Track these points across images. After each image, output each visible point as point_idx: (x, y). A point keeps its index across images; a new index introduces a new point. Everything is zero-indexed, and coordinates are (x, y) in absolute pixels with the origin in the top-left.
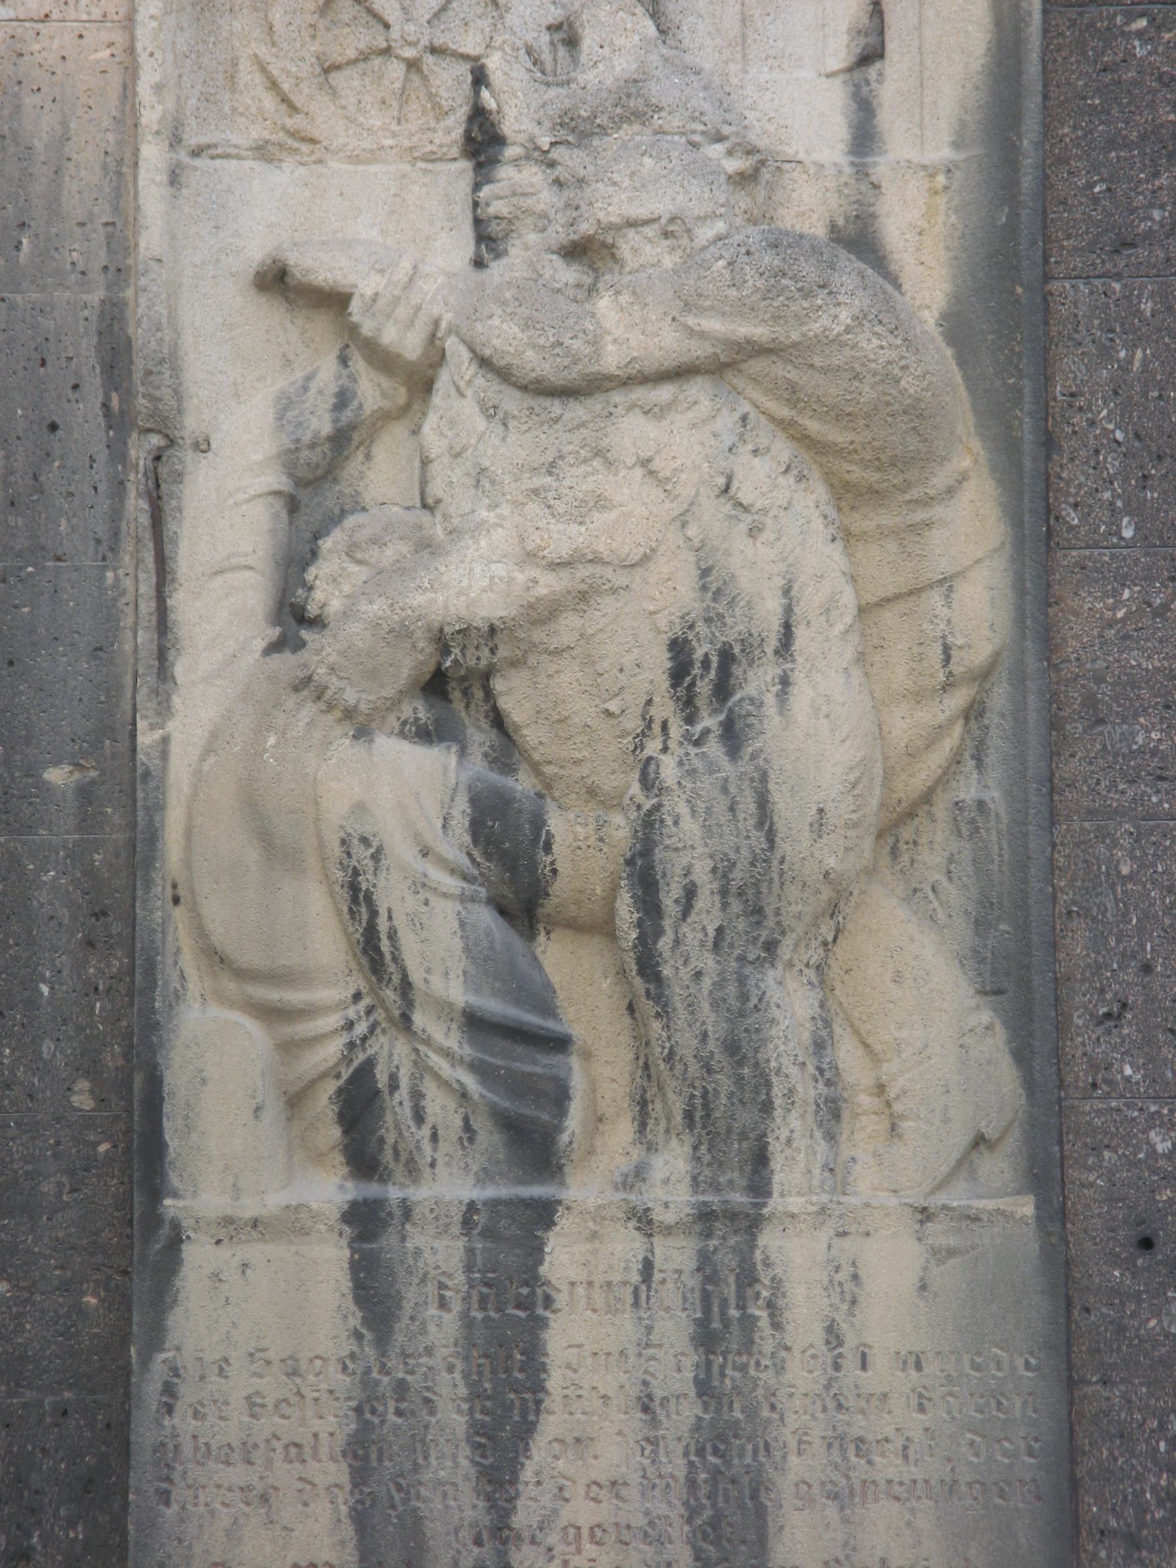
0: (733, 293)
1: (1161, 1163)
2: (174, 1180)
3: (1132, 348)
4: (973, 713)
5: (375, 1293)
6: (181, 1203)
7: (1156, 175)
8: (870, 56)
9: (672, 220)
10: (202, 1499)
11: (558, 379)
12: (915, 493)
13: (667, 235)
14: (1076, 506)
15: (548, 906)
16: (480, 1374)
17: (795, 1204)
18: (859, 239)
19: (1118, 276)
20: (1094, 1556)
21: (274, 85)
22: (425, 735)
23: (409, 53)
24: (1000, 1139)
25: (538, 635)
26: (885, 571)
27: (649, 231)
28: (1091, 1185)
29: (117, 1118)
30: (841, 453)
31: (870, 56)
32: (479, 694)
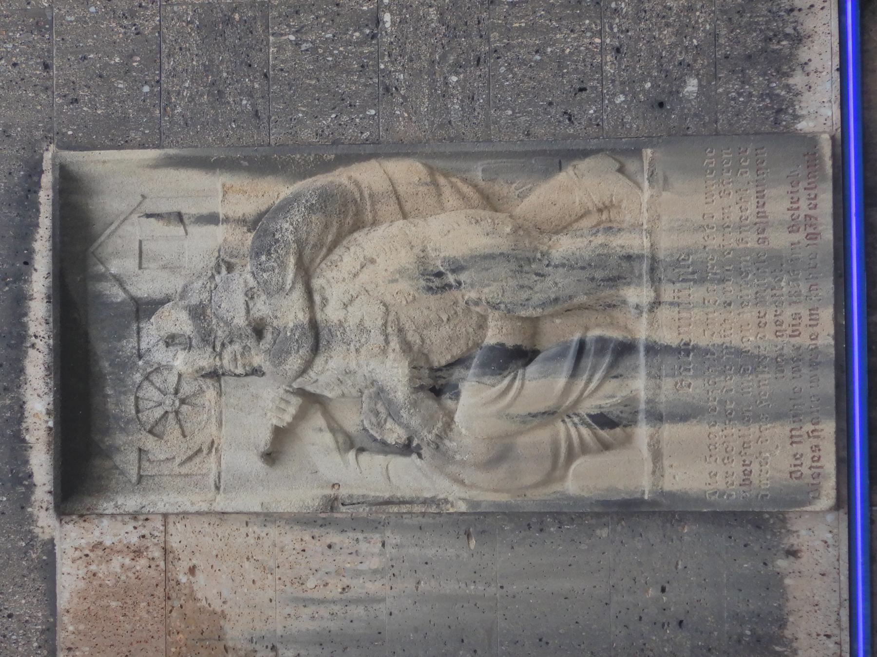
0: (276, 271)
1: (629, 99)
2: (638, 496)
3: (298, 111)
4: (446, 175)
5: (684, 414)
6: (647, 492)
7: (229, 103)
8: (179, 217)
9: (246, 295)
10: (765, 482)
11: (311, 341)
12: (357, 196)
13: (252, 298)
14: (362, 133)
15: (526, 345)
16: (716, 371)
17: (646, 243)
18: (256, 223)
19: (269, 117)
20: (785, 126)
21: (190, 458)
22: (457, 396)
23: (177, 403)
24: (620, 162)
25: (416, 348)
26: (388, 208)
27: (251, 305)
28: (638, 126)
29: (612, 518)
30: (341, 226)
31: (179, 217)
32: (439, 374)
